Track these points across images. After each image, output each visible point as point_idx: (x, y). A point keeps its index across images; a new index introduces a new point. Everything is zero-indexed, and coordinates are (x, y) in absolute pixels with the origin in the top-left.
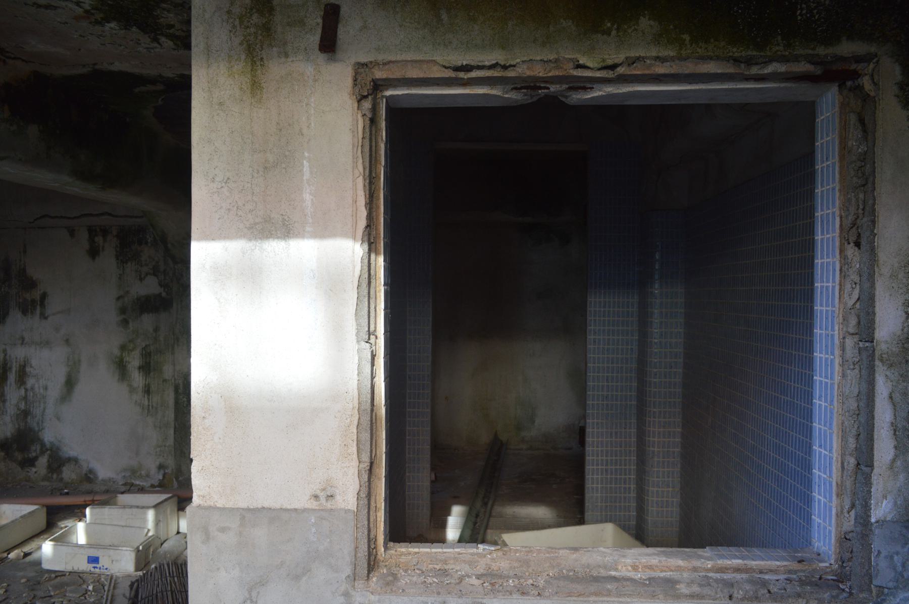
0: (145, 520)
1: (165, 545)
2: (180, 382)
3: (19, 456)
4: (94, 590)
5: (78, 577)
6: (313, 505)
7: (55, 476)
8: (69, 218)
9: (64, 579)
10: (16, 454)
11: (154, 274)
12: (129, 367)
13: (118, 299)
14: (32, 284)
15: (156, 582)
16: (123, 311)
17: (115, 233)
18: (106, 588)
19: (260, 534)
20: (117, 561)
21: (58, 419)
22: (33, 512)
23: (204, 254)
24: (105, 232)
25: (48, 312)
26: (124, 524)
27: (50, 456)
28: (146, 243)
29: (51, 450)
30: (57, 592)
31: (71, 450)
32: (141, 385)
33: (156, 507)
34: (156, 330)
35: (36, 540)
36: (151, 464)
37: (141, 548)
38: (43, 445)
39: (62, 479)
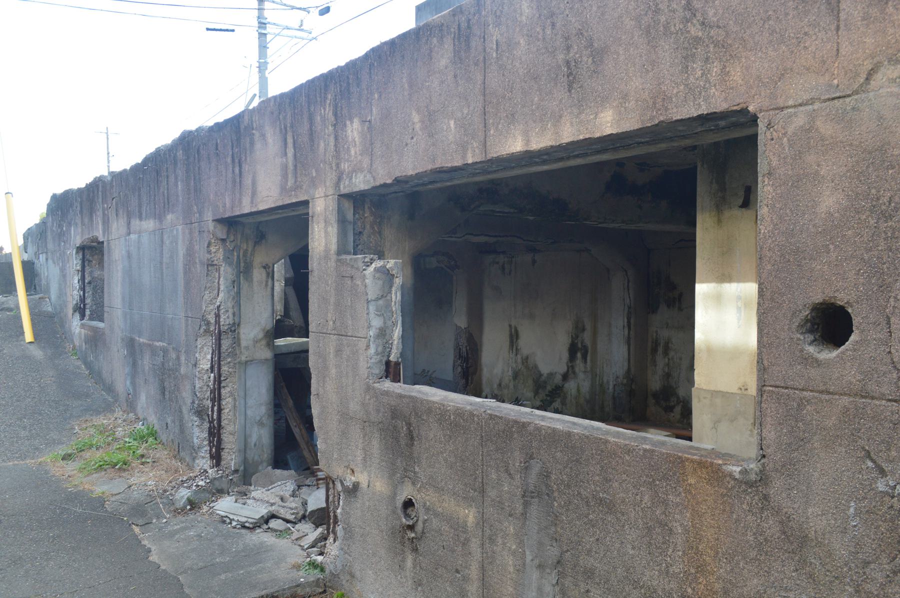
6: (739, 392)
19: (718, 401)
23: (701, 289)
38: (678, 398)
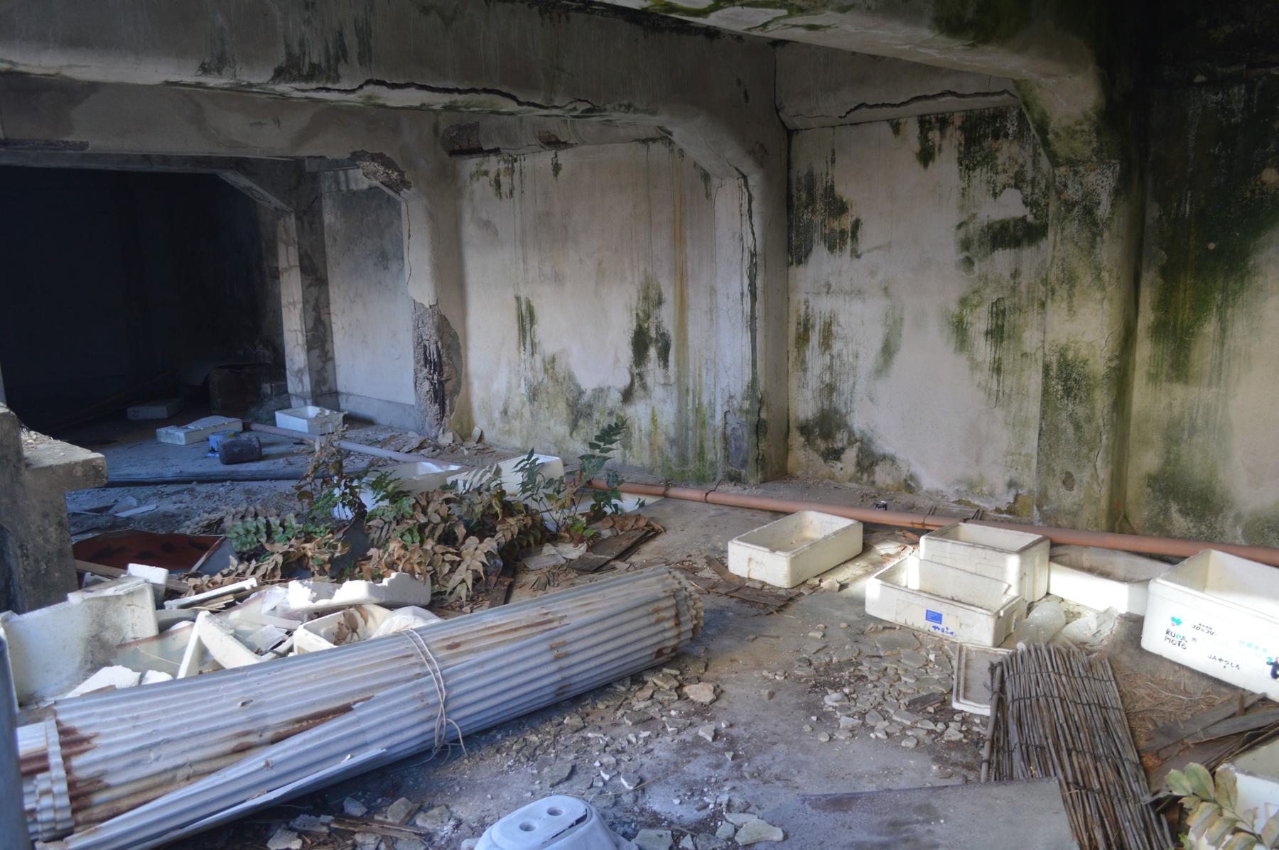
0: (1003, 570)
1: (1035, 614)
2: (1054, 359)
3: (821, 444)
4: (937, 662)
5: (912, 638)
7: (865, 477)
8: (894, 105)
9: (895, 635)
10: (819, 441)
11: (1017, 186)
12: (972, 331)
13: (960, 226)
14: (838, 208)
15: (1033, 677)
16: (966, 245)
17: (958, 122)
18: (955, 663)
20: (967, 625)
21: (872, 400)
22: (847, 528)
24: (943, 122)
25: (863, 246)
26: (973, 570)
27: (860, 450)
28: (1006, 136)
29: (861, 441)
30: (888, 653)
31: (884, 445)
32: (988, 359)
33: (1022, 552)
34: (1015, 274)
35: (850, 565)
36: (997, 479)
37: (1002, 613)
38: (851, 433)
39: (873, 483)
